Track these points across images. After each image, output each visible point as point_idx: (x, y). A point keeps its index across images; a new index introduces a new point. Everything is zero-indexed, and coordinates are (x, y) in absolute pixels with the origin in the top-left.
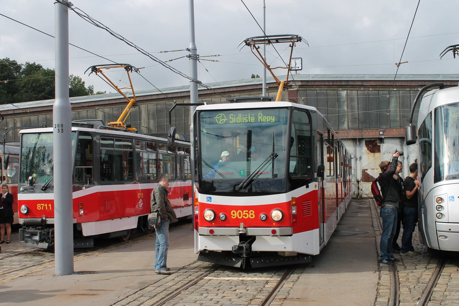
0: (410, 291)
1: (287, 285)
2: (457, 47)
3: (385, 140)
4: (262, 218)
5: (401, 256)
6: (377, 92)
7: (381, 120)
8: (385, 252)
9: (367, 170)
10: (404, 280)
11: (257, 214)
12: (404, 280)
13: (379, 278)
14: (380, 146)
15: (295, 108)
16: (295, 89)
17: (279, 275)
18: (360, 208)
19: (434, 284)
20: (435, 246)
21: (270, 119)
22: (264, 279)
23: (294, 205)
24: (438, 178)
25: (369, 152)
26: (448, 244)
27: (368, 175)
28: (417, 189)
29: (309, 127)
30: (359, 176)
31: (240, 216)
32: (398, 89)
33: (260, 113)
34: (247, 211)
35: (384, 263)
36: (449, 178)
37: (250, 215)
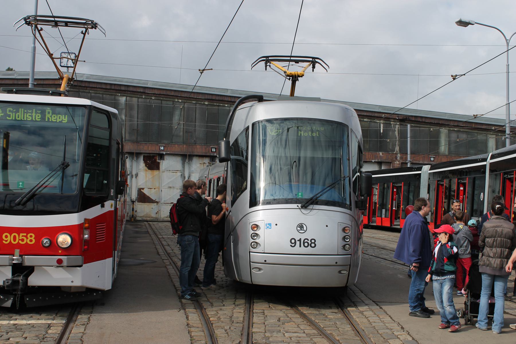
0: (227, 333)
1: (76, 330)
2: (270, 58)
3: (166, 157)
4: (44, 243)
5: (202, 290)
6: (160, 101)
7: (163, 134)
8: (187, 286)
9: (143, 189)
10: (216, 319)
11: (38, 238)
12: (216, 319)
13: (187, 318)
14: (159, 163)
15: (95, 107)
17: (63, 316)
18: (137, 232)
19: (250, 324)
20: (246, 279)
21: (63, 119)
22: (43, 322)
23: (87, 228)
24: (254, 202)
25: (147, 169)
26: (261, 277)
27: (144, 194)
28: (225, 213)
29: (107, 133)
30: (134, 195)
31: (15, 240)
32: (183, 101)
33: (48, 109)
34: (25, 234)
35: (187, 299)
36: (267, 202)
37: (28, 240)
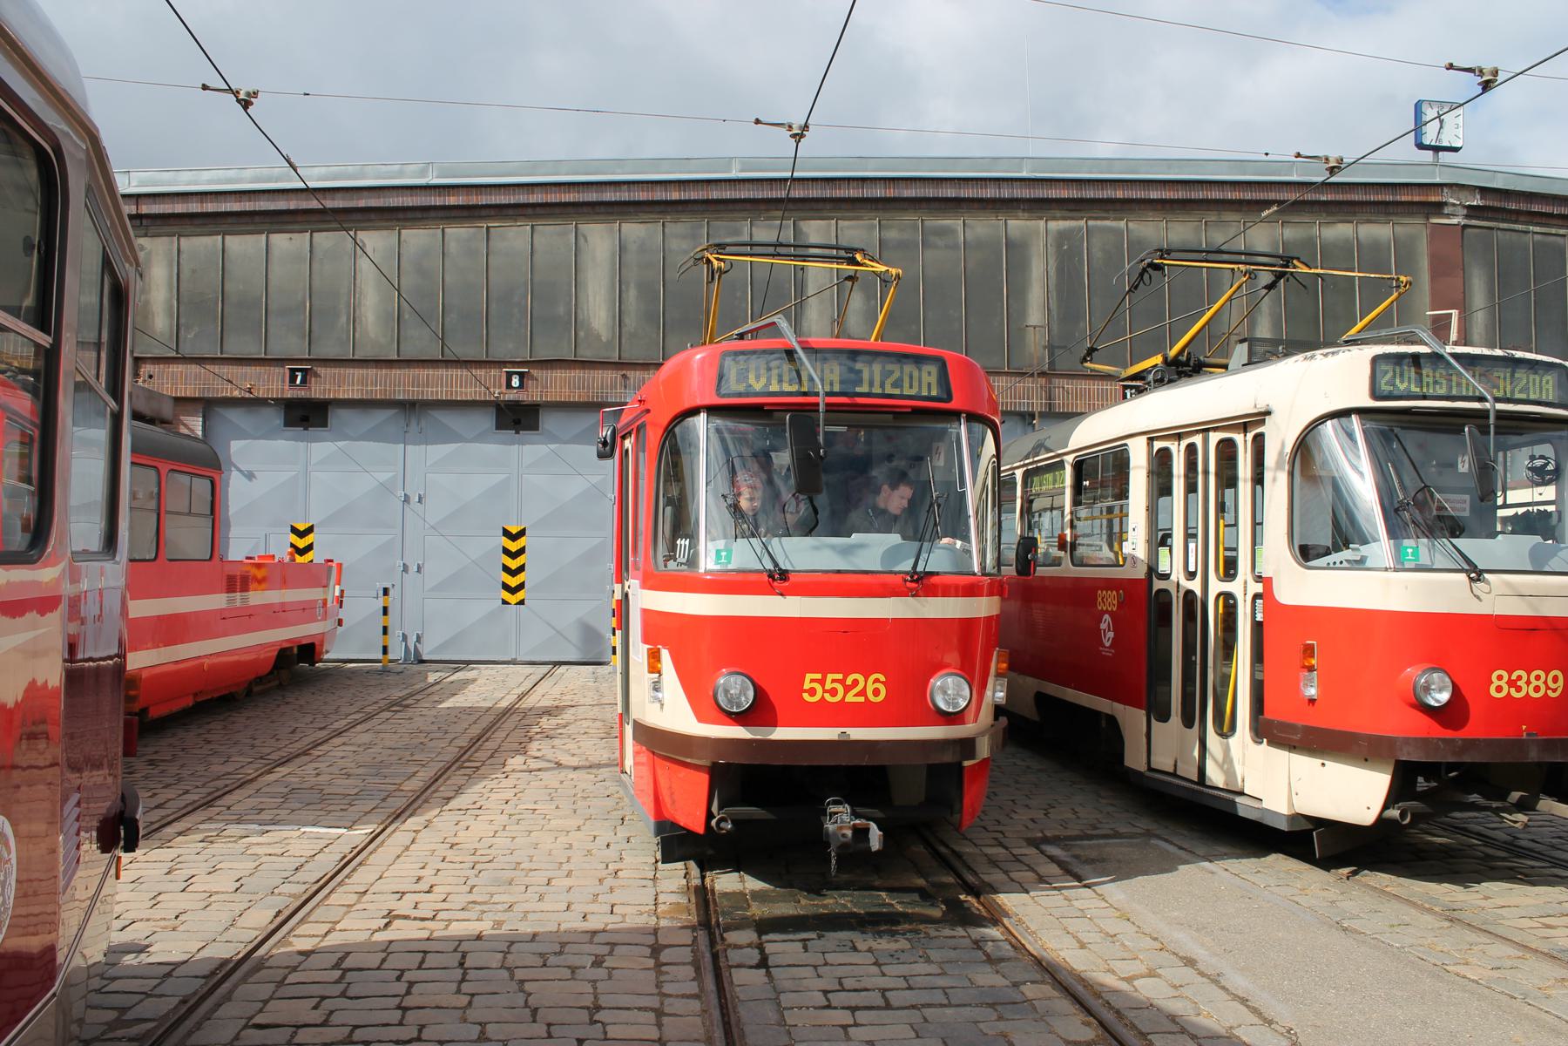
16: (1455, 221)
34: (819, 676)
37: (1531, 687)
